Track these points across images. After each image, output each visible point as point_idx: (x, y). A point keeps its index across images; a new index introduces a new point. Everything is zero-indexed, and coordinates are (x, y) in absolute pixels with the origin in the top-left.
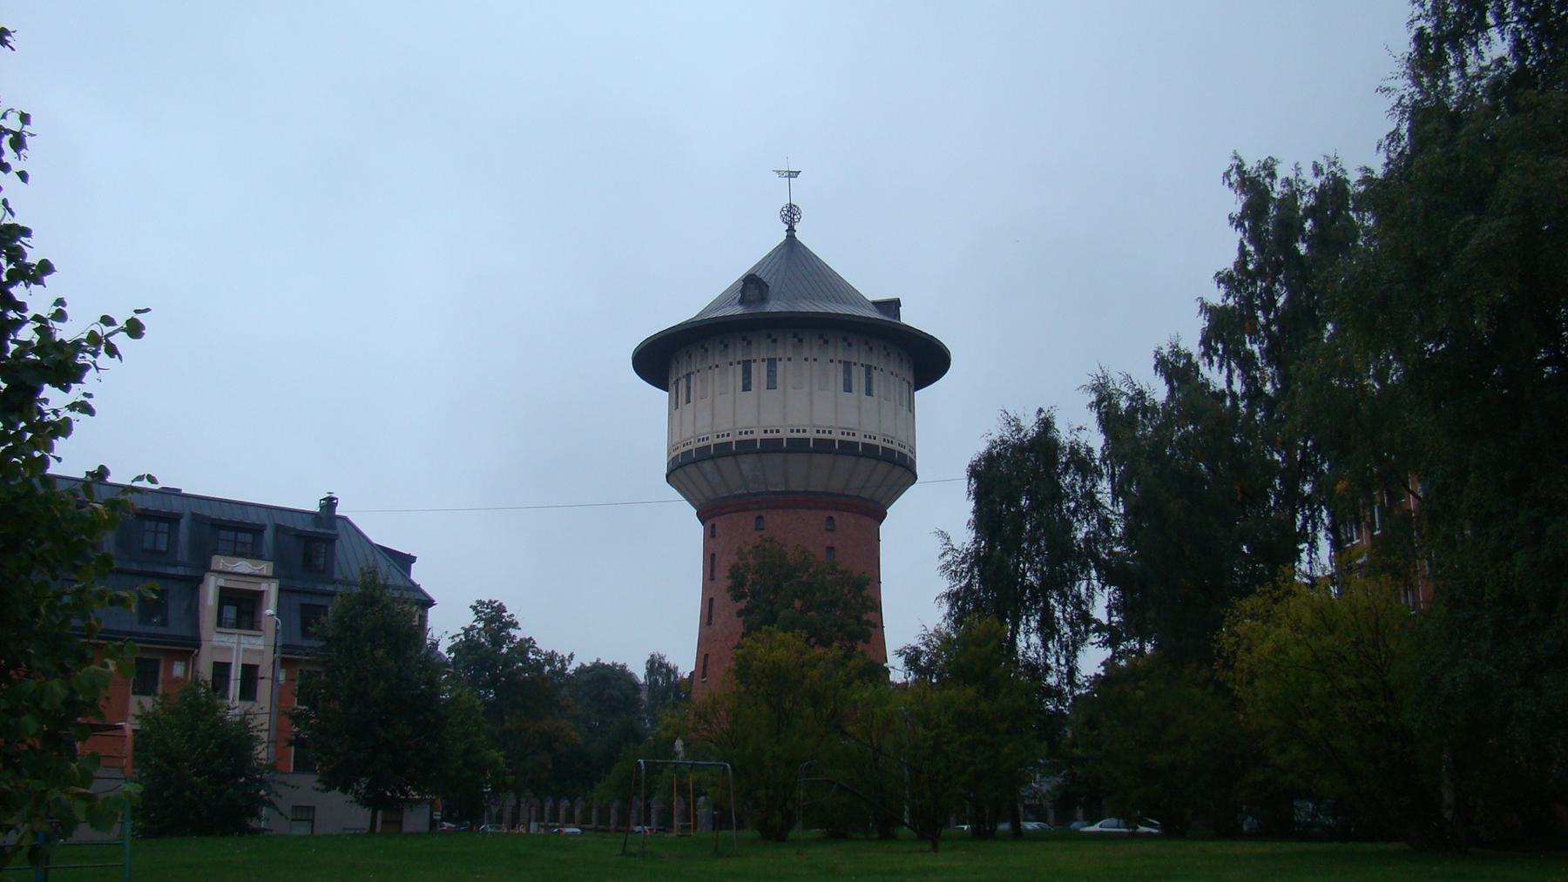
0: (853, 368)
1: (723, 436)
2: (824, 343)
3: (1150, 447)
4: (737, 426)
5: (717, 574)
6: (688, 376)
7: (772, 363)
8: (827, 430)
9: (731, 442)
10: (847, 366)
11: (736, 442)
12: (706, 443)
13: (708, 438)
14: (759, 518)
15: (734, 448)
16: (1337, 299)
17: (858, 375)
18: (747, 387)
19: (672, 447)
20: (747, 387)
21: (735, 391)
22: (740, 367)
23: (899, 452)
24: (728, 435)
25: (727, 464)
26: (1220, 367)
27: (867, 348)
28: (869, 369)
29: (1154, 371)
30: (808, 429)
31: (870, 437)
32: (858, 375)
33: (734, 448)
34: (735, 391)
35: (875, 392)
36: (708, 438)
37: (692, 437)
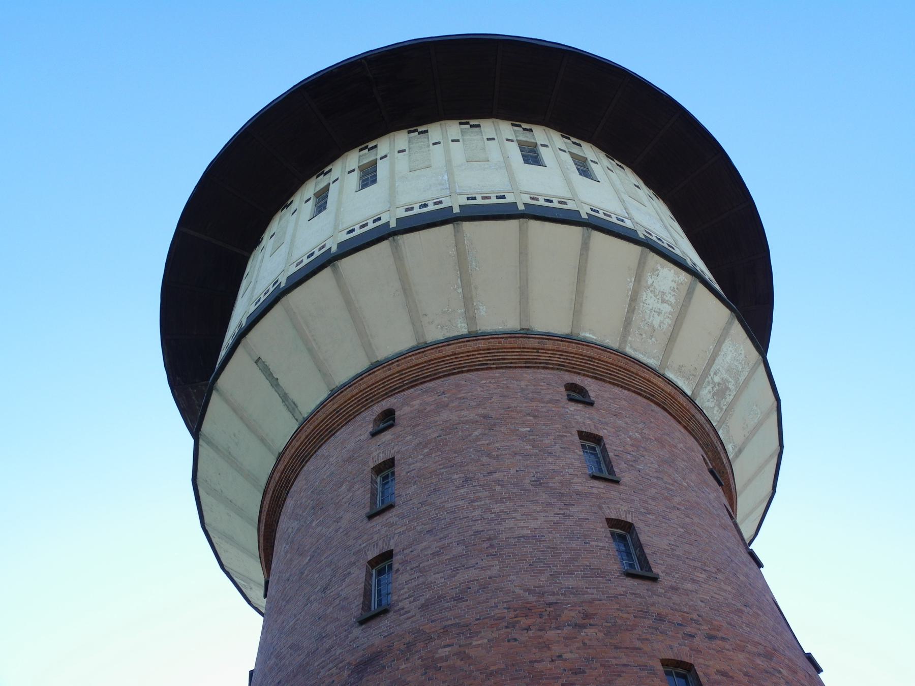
19: (331, 175)
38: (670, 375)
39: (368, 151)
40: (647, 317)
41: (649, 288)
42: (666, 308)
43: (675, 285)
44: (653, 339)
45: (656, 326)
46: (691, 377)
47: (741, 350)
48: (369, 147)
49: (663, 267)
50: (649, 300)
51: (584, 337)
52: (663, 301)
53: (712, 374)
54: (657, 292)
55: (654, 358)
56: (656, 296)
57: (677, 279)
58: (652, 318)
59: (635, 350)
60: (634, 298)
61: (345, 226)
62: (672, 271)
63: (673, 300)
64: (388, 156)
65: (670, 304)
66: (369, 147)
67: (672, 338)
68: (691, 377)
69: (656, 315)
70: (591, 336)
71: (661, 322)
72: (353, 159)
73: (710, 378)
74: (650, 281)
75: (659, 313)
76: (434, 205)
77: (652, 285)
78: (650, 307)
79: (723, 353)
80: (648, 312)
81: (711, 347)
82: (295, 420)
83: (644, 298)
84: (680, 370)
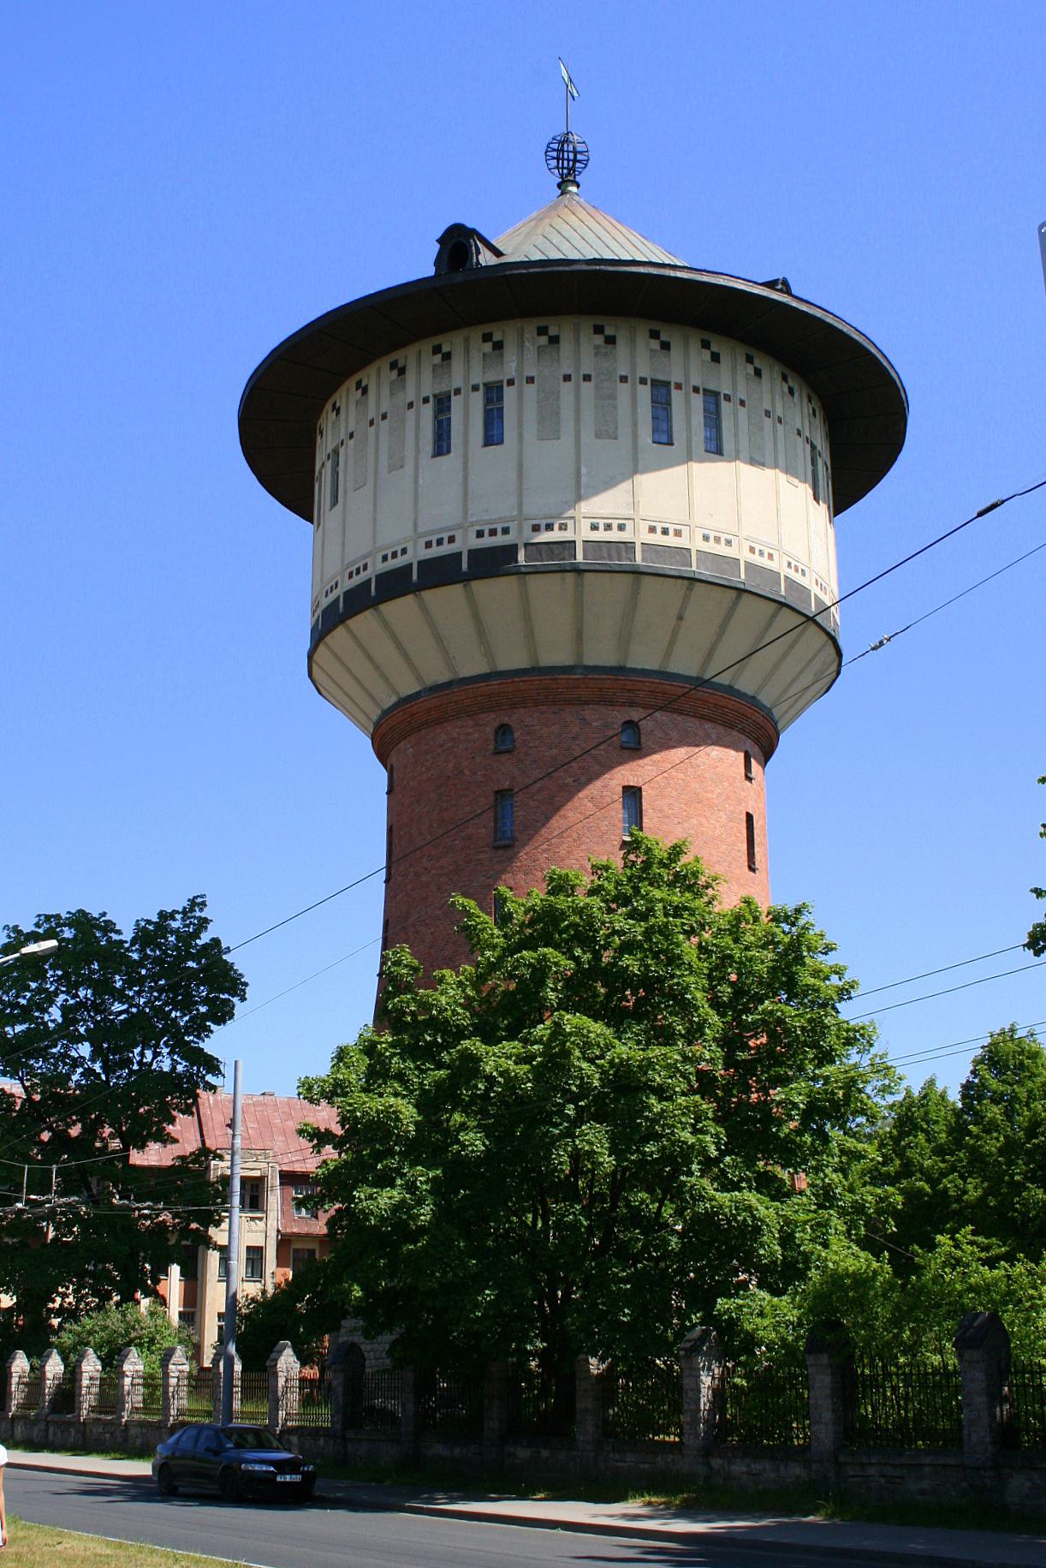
0: (677, 397)
1: (394, 555)
2: (662, 348)
3: (912, 1288)
6: (336, 452)
7: (493, 394)
8: (615, 524)
9: (460, 554)
10: (661, 391)
11: (470, 552)
12: (401, 561)
13: (404, 551)
14: (504, 730)
15: (415, 577)
16: (155, 994)
17: (688, 413)
18: (442, 445)
19: (316, 604)
20: (442, 445)
22: (428, 411)
23: (786, 577)
24: (452, 540)
25: (446, 600)
26: (801, 396)
27: (707, 355)
28: (713, 399)
29: (815, 503)
30: (513, 526)
31: (717, 540)
32: (468, 415)
33: (415, 577)
35: (728, 444)
36: (506, 531)
37: (460, 527)
39: (399, 375)
72: (351, 383)
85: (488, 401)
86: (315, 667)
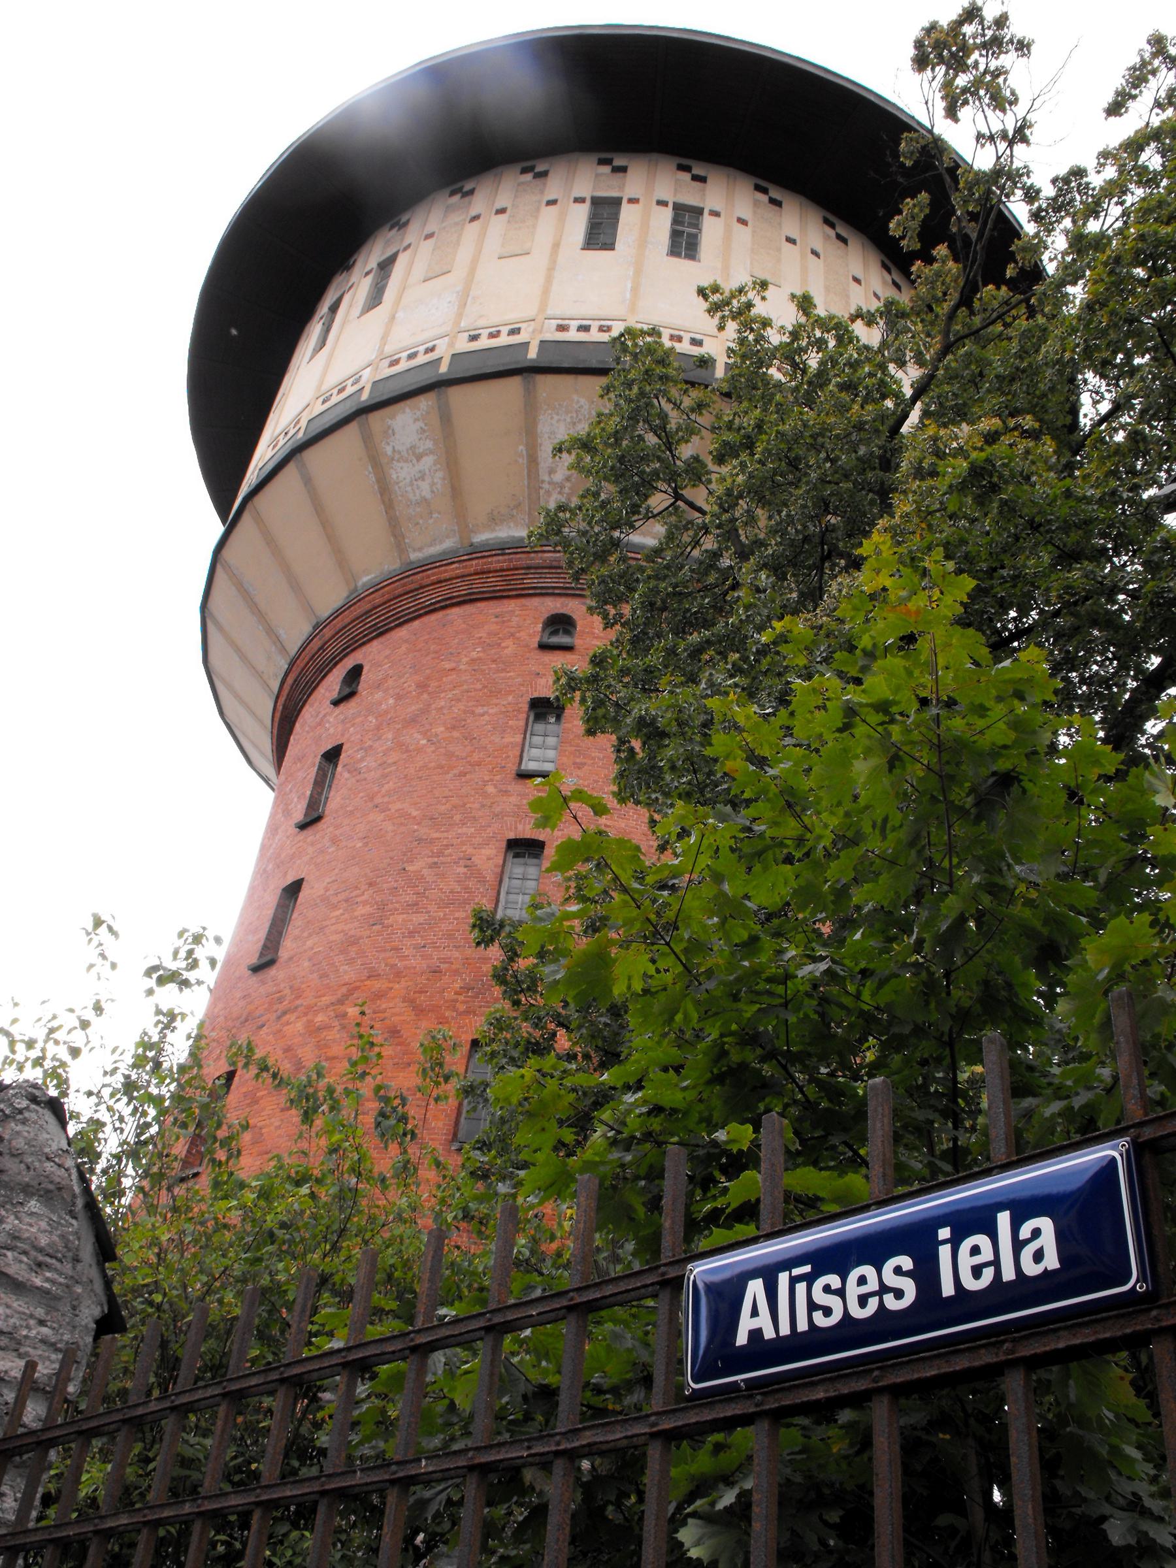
4: (550, 312)
5: (335, 801)
21: (556, 246)
34: (556, 246)
38: (482, 537)
40: (411, 496)
41: (393, 459)
42: (428, 461)
43: (420, 424)
44: (435, 515)
45: (428, 496)
46: (515, 512)
47: (578, 402)
48: (538, 169)
49: (393, 417)
50: (402, 473)
51: (364, 585)
52: (419, 458)
53: (546, 478)
54: (405, 454)
55: (448, 537)
56: (406, 461)
57: (418, 413)
58: (417, 492)
59: (420, 549)
60: (384, 489)
61: (558, 312)
62: (407, 410)
63: (429, 444)
64: (509, 211)
65: (431, 452)
66: (538, 169)
67: (456, 490)
68: (515, 512)
69: (420, 483)
70: (369, 577)
71: (433, 484)
73: (546, 486)
74: (389, 450)
75: (422, 478)
76: (609, 246)
77: (394, 450)
78: (408, 480)
79: (546, 436)
80: (409, 489)
81: (521, 447)
82: (115, 928)
83: (394, 476)
84: (494, 520)
85: (676, 221)
86: (219, 569)
